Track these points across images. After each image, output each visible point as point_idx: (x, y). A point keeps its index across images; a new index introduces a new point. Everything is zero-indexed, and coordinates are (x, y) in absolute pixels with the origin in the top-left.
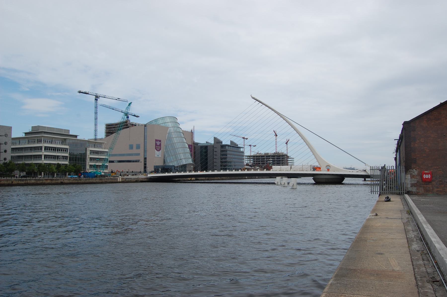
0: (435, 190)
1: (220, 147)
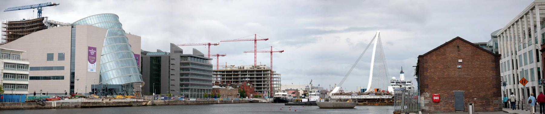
0: (443, 108)
1: (179, 57)
